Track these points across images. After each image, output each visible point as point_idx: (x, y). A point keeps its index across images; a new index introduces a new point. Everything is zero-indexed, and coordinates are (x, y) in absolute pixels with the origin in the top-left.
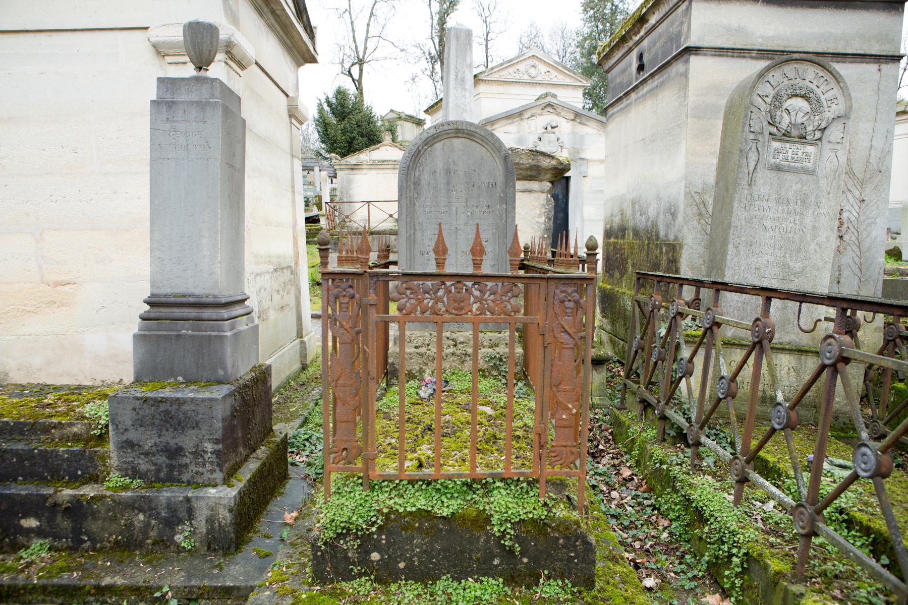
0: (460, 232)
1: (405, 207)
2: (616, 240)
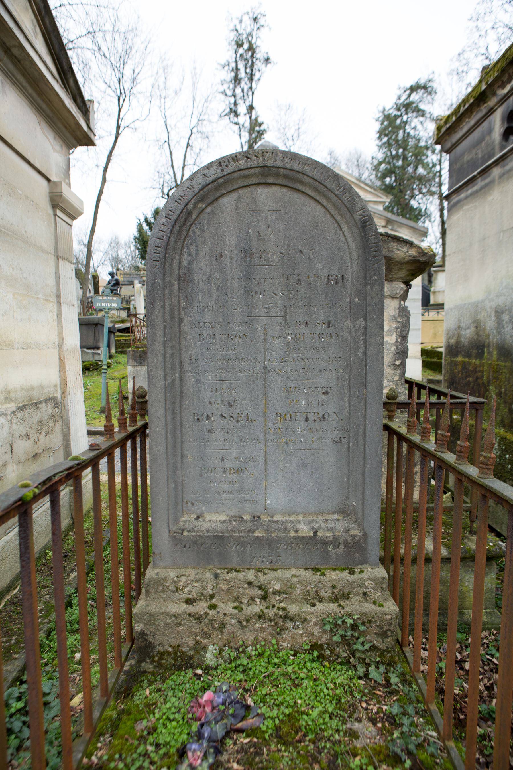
0: (272, 376)
1: (160, 327)
2: (467, 360)
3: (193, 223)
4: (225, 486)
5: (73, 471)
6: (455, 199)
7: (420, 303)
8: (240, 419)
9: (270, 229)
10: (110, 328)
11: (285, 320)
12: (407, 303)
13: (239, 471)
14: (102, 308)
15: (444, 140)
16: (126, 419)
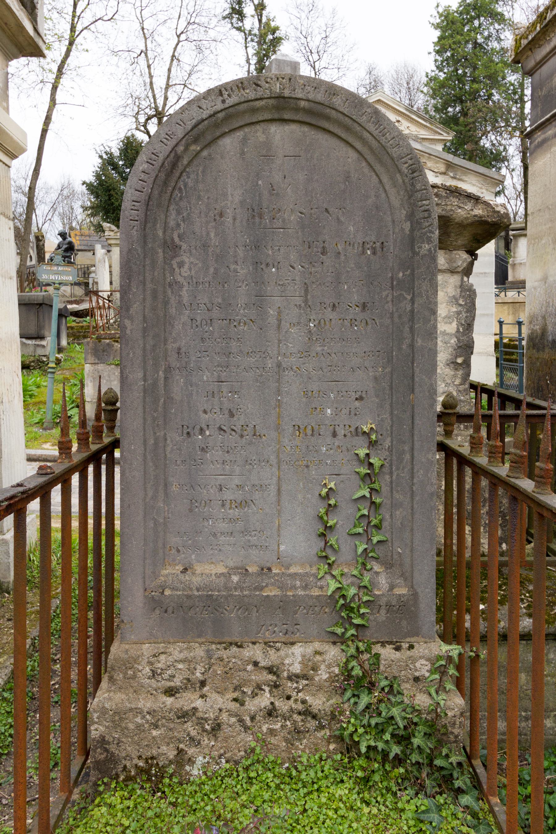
0: (288, 375)
3: (184, 170)
4: (223, 526)
5: (16, 502)
6: (539, 137)
7: (492, 279)
8: (246, 433)
9: (286, 180)
10: (60, 310)
11: (306, 301)
12: (472, 279)
13: (243, 504)
14: (49, 281)
15: (525, 57)
16: (88, 433)
